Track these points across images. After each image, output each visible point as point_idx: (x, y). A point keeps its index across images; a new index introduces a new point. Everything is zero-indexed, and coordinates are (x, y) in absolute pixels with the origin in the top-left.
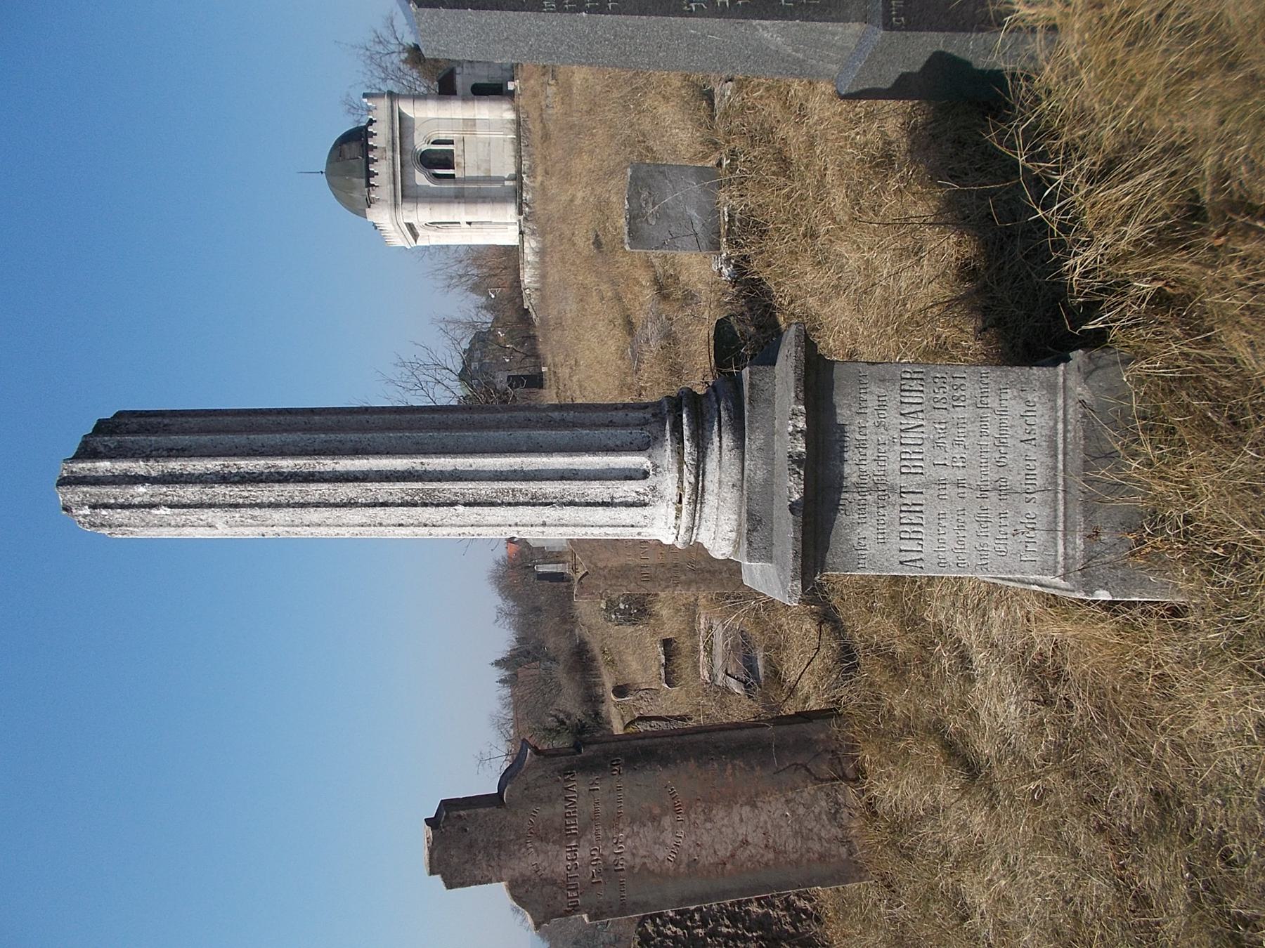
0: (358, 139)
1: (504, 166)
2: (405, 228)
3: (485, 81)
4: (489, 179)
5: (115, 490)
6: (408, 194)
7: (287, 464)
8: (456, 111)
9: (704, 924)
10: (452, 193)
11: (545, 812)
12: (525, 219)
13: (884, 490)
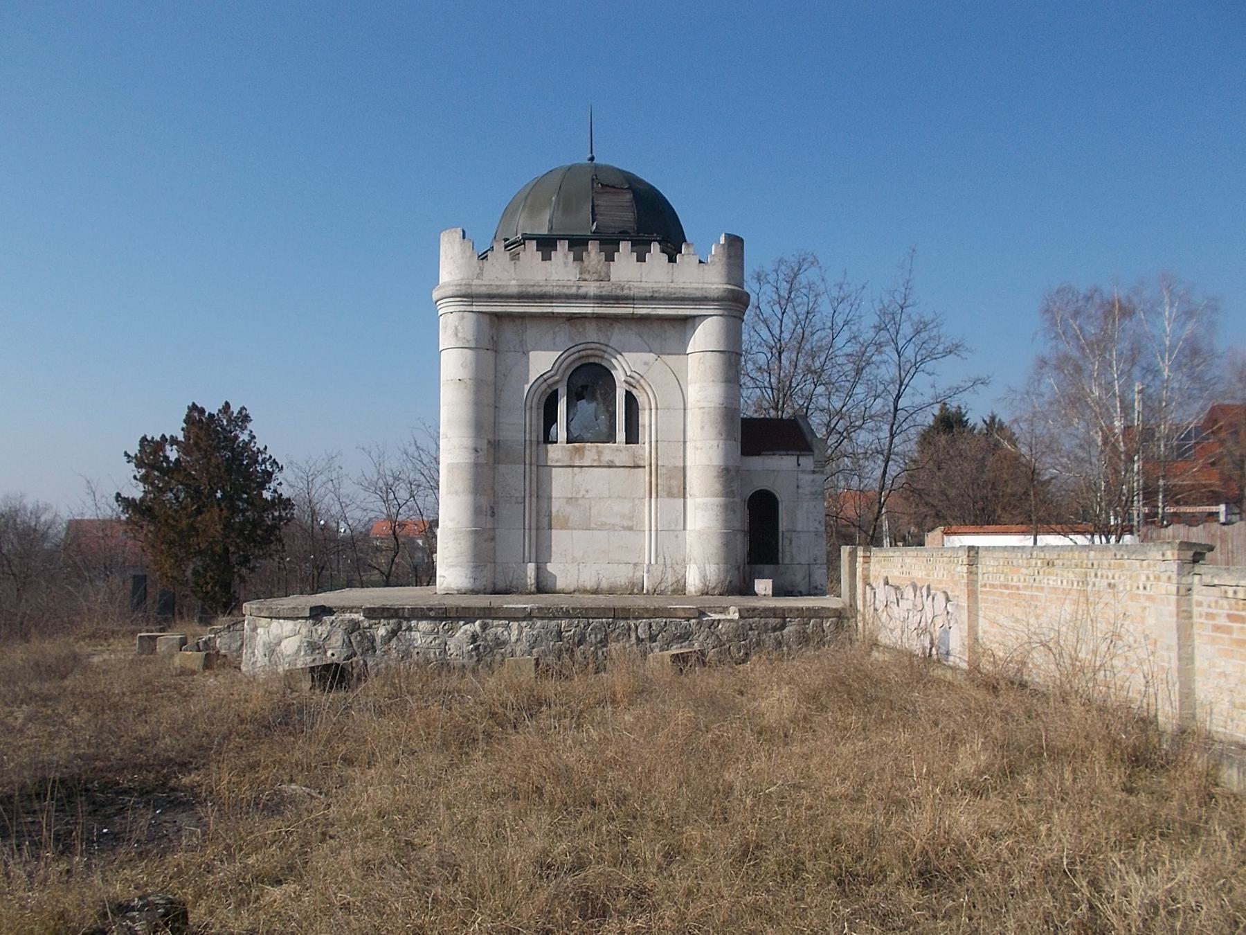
3: (783, 525)
6: (502, 327)
8: (702, 452)
12: (354, 627)
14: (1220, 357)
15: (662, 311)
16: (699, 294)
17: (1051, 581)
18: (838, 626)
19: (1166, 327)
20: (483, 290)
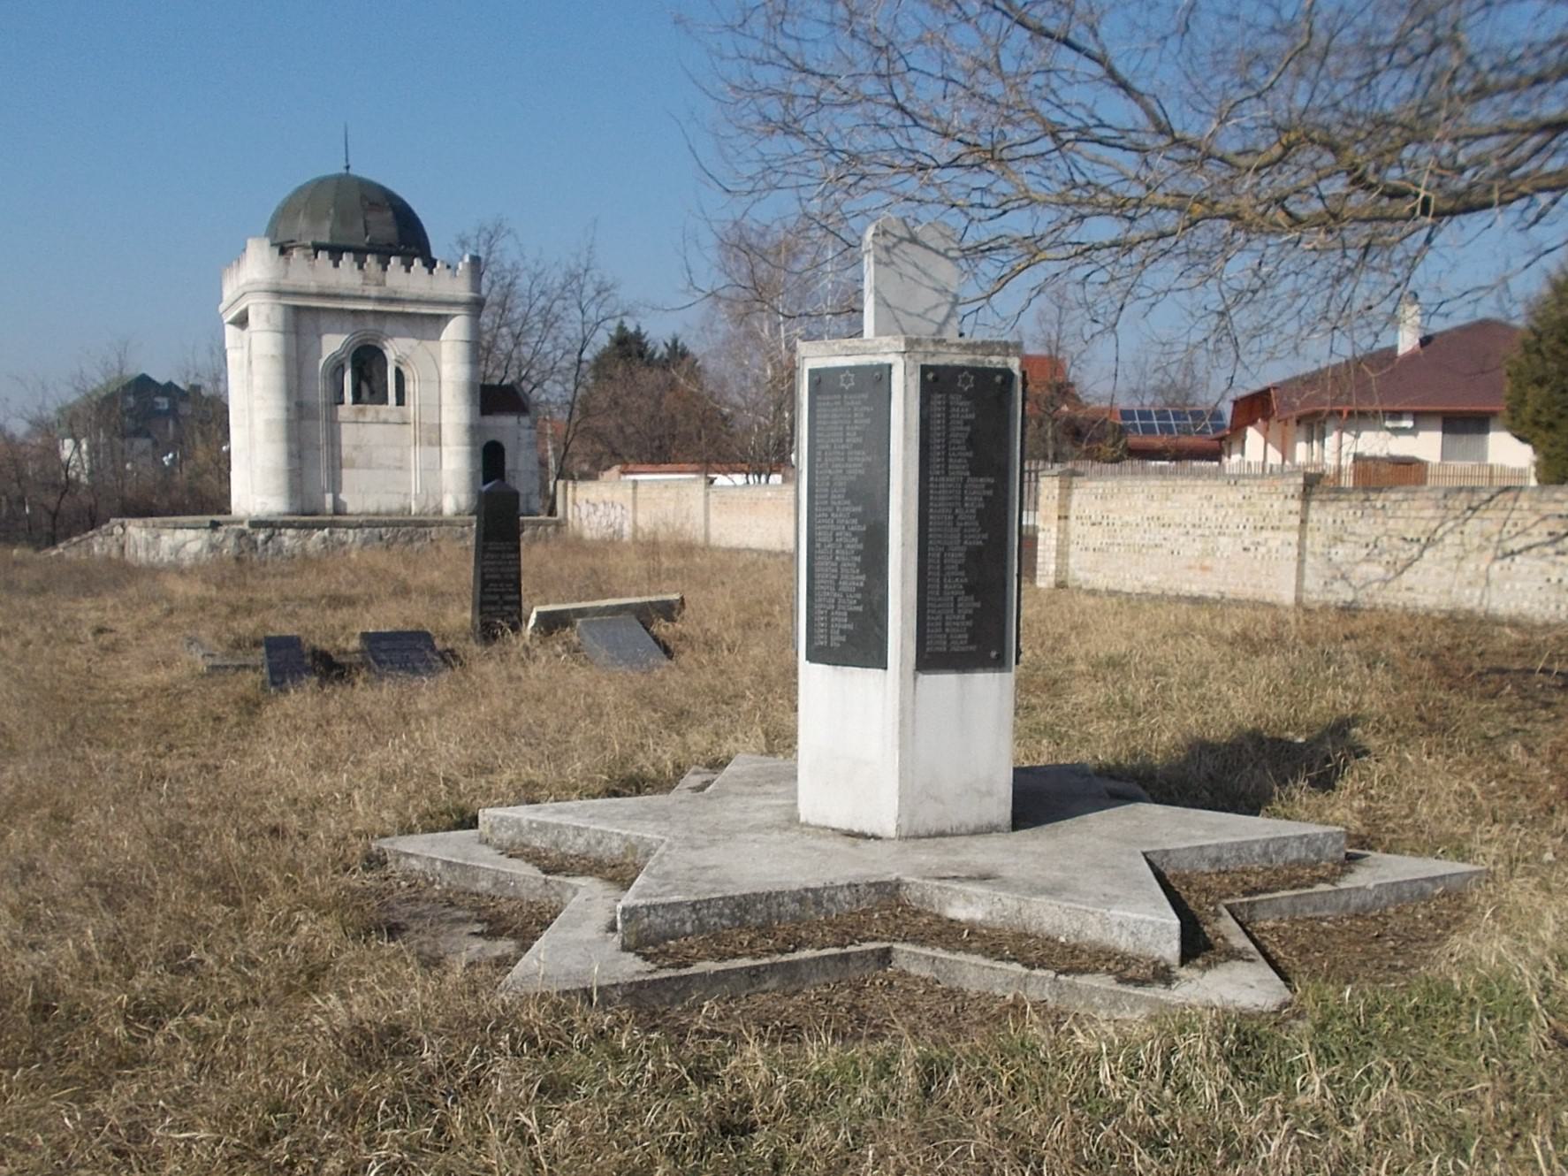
0: (408, 239)
1: (362, 493)
4: (336, 465)
6: (301, 320)
8: (454, 413)
12: (242, 534)
15: (425, 310)
17: (667, 495)
18: (557, 531)
20: (290, 289)
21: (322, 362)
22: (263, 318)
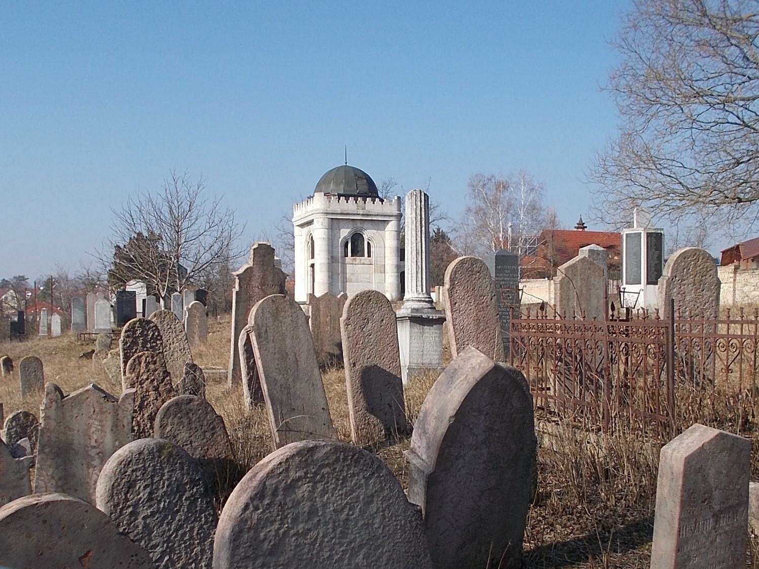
0: (370, 191)
2: (309, 219)
4: (344, 281)
5: (419, 199)
6: (334, 223)
7: (423, 229)
9: (151, 347)
10: (335, 254)
11: (270, 278)
13: (423, 333)
14: (544, 210)
16: (391, 214)
19: (522, 196)
20: (331, 212)
21: (340, 240)
22: (320, 223)
